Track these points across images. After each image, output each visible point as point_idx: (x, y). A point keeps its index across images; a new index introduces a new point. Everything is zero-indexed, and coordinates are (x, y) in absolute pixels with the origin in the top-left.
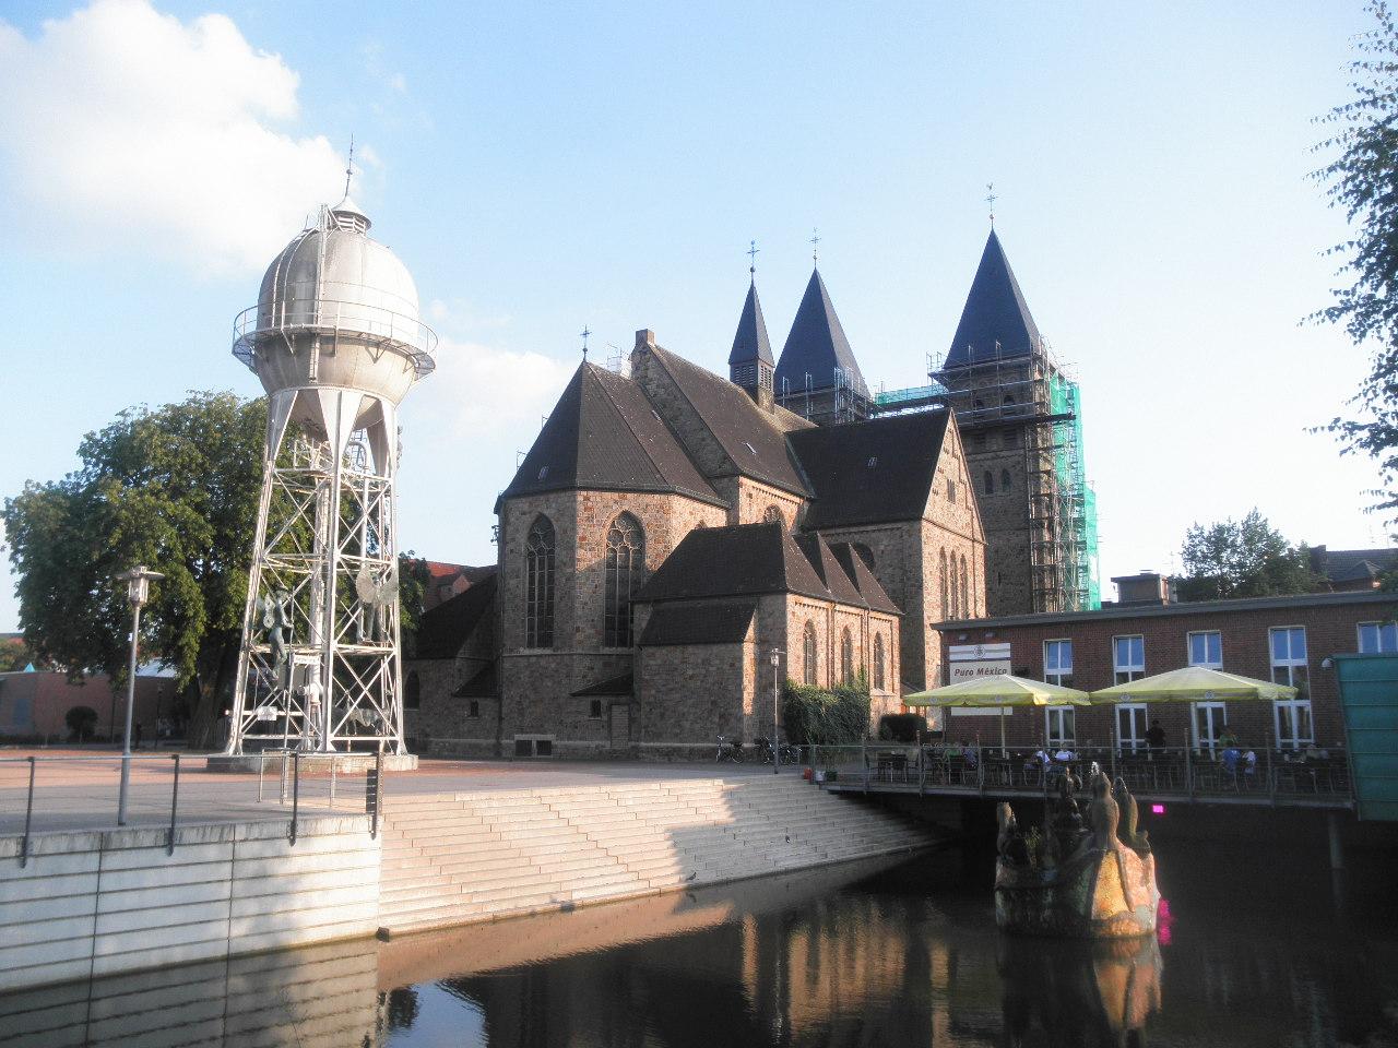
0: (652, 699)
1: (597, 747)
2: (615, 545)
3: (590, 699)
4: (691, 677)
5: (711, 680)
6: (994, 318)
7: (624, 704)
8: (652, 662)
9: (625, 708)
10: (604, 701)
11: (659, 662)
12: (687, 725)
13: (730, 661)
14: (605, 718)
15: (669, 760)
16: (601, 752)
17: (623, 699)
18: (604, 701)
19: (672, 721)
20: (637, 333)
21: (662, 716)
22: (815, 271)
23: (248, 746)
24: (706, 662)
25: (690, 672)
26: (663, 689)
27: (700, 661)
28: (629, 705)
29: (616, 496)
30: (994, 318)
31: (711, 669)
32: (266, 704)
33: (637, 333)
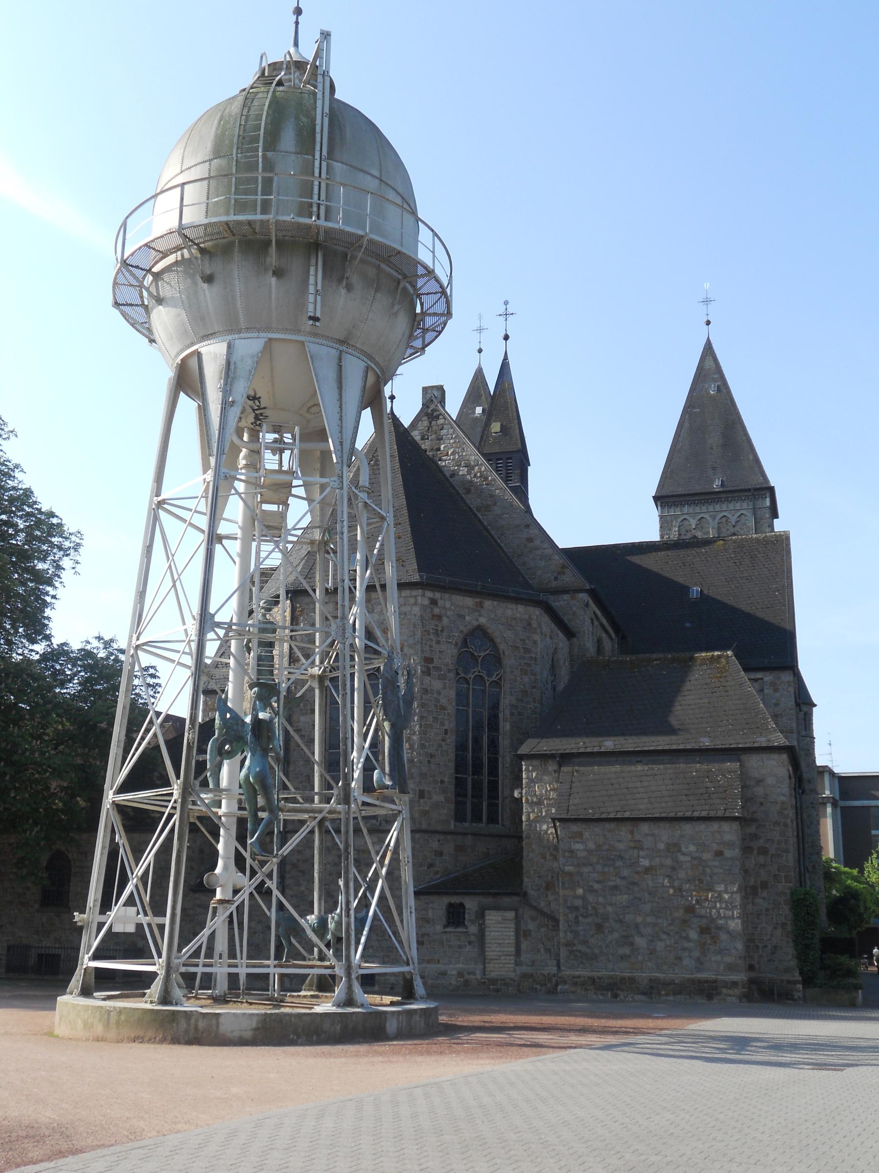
0: (578, 903)
1: (460, 974)
2: (466, 673)
3: (446, 900)
4: (648, 870)
5: (682, 875)
6: (713, 458)
7: (506, 909)
8: (579, 846)
9: (511, 915)
10: (471, 904)
11: (591, 845)
12: (640, 942)
13: (715, 847)
14: (473, 929)
15: (615, 996)
16: (466, 983)
17: (506, 900)
18: (471, 904)
19: (616, 935)
20: (425, 390)
21: (599, 927)
22: (708, 350)
23: (408, 964)
24: (673, 848)
25: (645, 863)
26: (597, 886)
27: (662, 846)
28: (516, 910)
29: (469, 601)
30: (713, 458)
31: (682, 858)
32: (136, 886)
33: (425, 390)
